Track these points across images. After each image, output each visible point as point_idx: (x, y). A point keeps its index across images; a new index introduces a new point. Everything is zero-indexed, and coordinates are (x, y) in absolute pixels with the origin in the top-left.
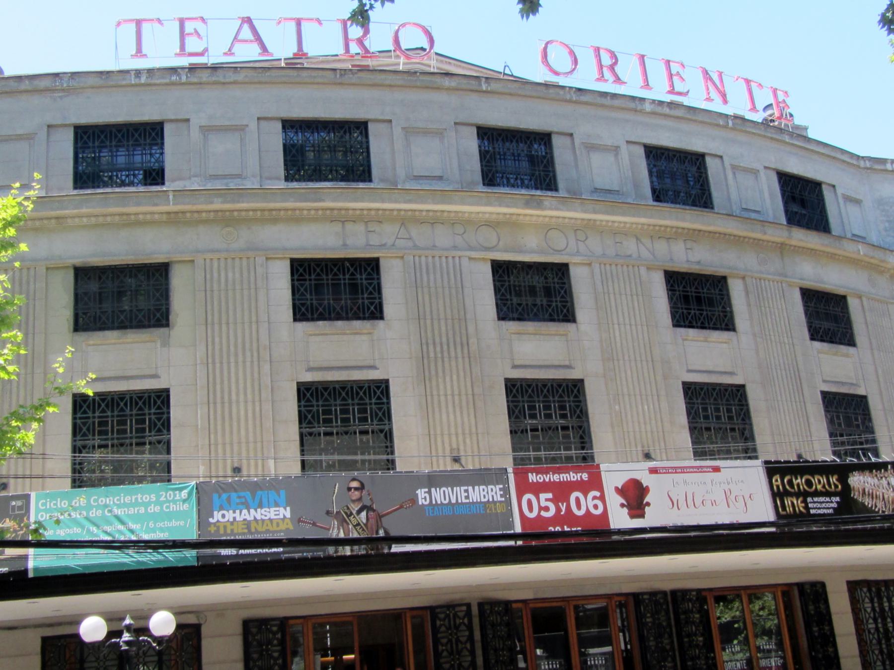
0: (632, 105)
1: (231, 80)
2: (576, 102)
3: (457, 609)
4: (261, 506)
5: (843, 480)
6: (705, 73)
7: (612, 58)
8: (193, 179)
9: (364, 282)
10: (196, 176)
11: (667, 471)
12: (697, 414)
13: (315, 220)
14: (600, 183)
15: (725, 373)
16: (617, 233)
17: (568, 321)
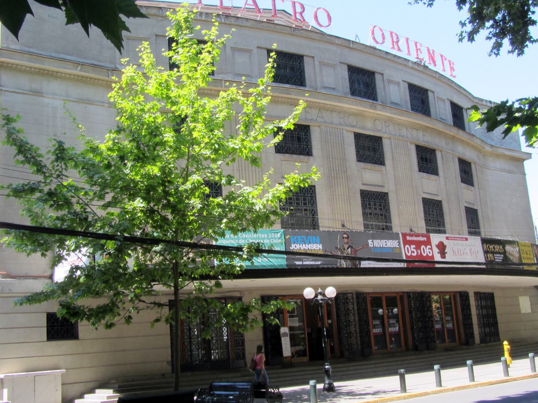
0: (404, 63)
1: (245, 25)
2: (385, 58)
3: (348, 295)
4: (310, 243)
5: (504, 247)
6: (428, 50)
7: (301, 8)
8: (229, 75)
9: (304, 137)
10: (230, 73)
11: (454, 239)
12: (426, 212)
13: (283, 103)
14: (393, 100)
15: (435, 195)
16: (400, 124)
17: (309, 155)
